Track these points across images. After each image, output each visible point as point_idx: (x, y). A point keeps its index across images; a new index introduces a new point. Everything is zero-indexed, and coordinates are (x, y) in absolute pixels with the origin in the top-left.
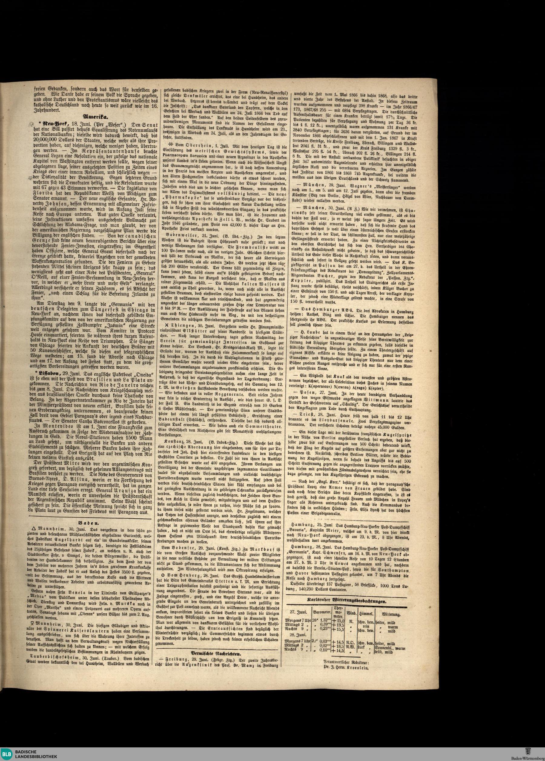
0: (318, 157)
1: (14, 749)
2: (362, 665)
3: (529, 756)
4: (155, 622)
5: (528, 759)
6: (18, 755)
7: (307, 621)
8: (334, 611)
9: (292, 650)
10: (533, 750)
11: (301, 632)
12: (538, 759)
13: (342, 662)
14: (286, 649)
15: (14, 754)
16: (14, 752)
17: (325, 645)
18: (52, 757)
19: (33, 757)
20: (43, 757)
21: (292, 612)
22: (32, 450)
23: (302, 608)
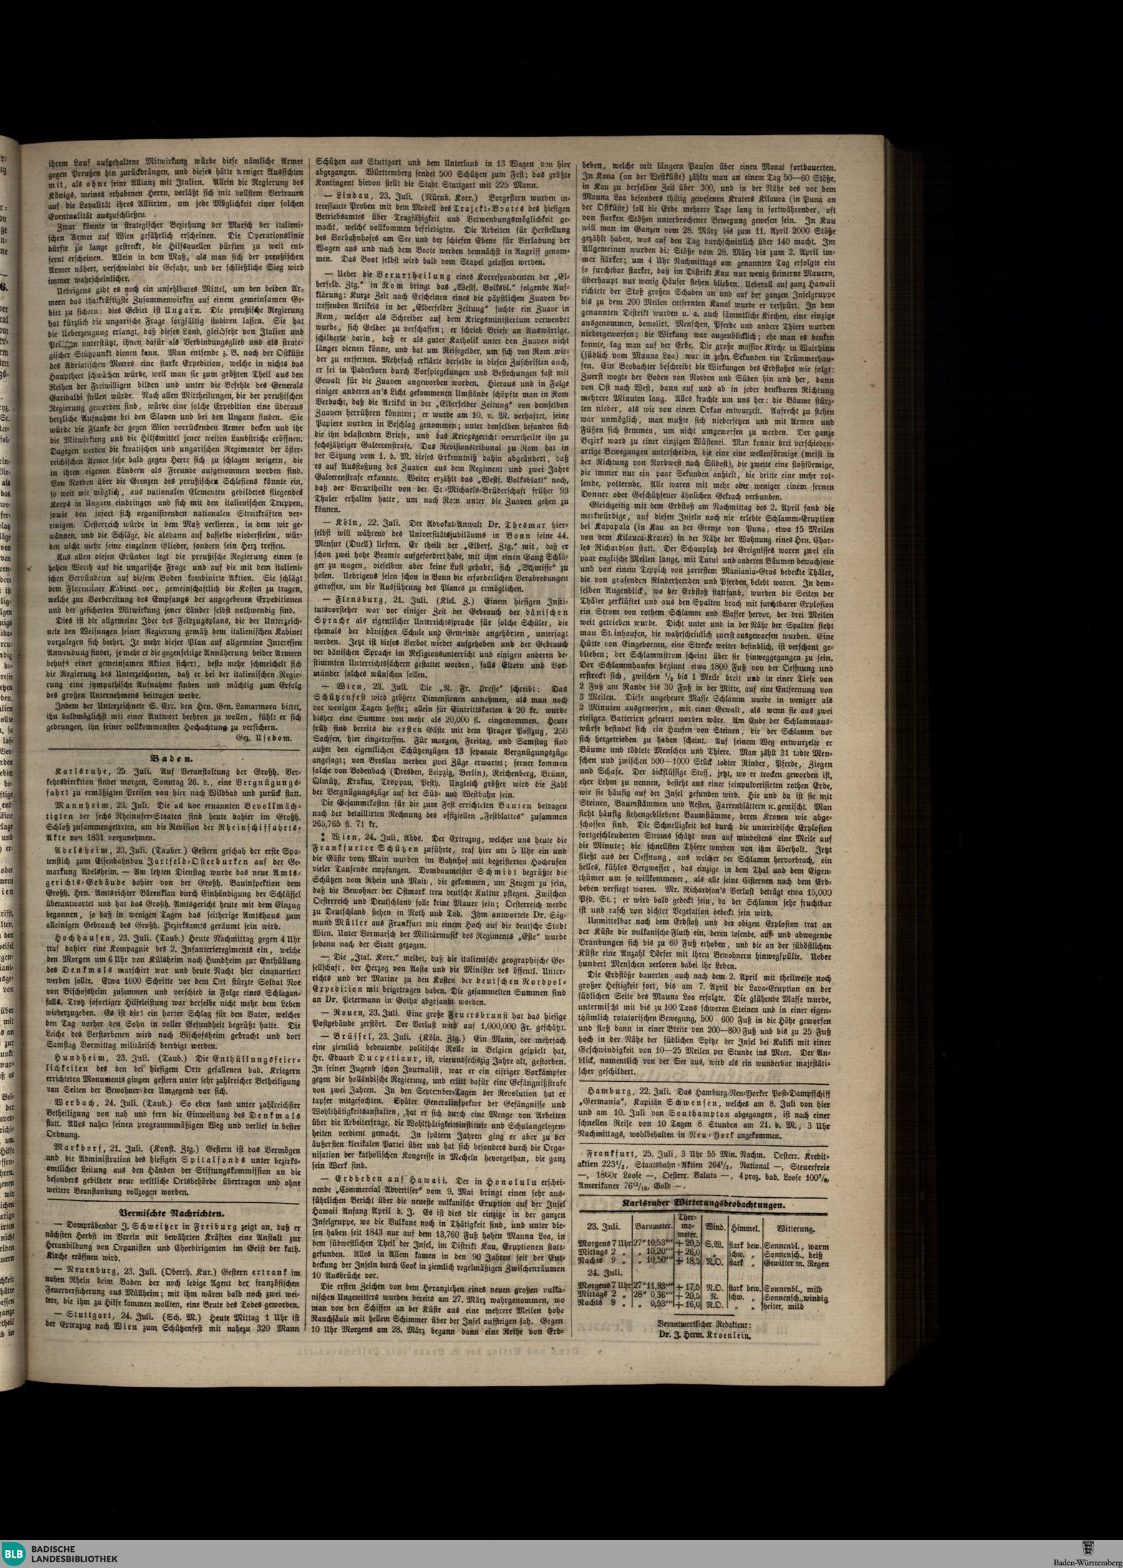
0: (632, 1008)
1: (28, 1544)
2: (740, 1331)
3: (1090, 1558)
4: (312, 544)
5: (1089, 1564)
6: (36, 1555)
7: (621, 1286)
8: (679, 1223)
9: (593, 1303)
10: (1099, 1545)
11: (612, 1268)
12: (1108, 1563)
13: (696, 1324)
14: (581, 1302)
15: (29, 1554)
16: (29, 1550)
17: (661, 1293)
18: (107, 1559)
19: (69, 1559)
20: (88, 1559)
21: (592, 1226)
22: (55, 414)
23: (610, 1219)
